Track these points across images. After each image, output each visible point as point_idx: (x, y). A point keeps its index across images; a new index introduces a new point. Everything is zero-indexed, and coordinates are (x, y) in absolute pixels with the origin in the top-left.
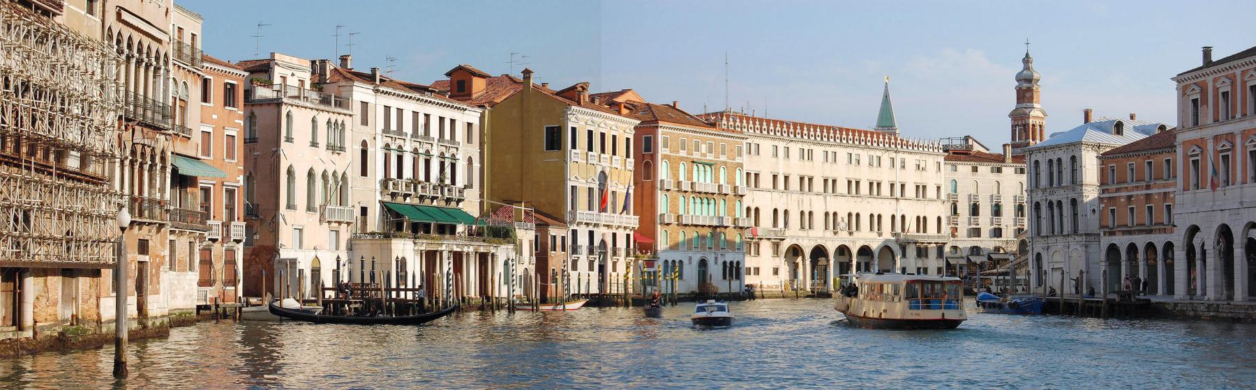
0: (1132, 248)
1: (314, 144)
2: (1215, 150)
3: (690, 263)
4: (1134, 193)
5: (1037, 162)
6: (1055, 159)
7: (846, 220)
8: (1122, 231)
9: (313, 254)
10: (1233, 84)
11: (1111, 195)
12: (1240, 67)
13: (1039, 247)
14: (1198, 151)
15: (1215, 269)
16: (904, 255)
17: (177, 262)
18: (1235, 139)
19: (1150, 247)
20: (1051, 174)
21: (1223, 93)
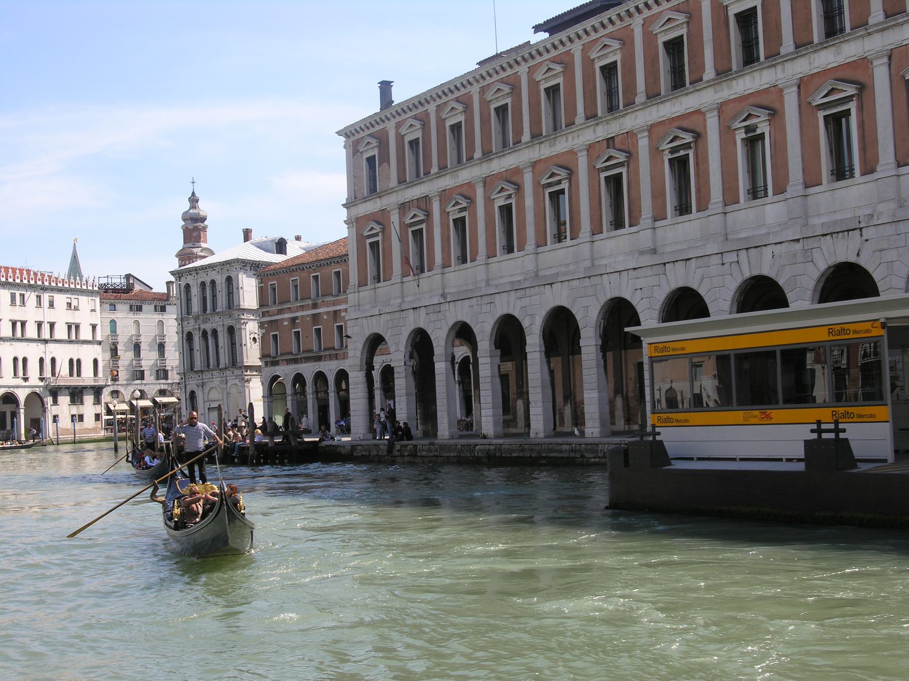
2: (402, 223)
4: (299, 314)
5: (188, 287)
8: (286, 360)
10: (425, 127)
11: (273, 318)
12: (435, 101)
13: (192, 385)
14: (378, 229)
15: (407, 394)
16: (55, 402)
17: (290, 420)
18: (431, 205)
19: (320, 377)
20: (204, 299)
21: (411, 143)
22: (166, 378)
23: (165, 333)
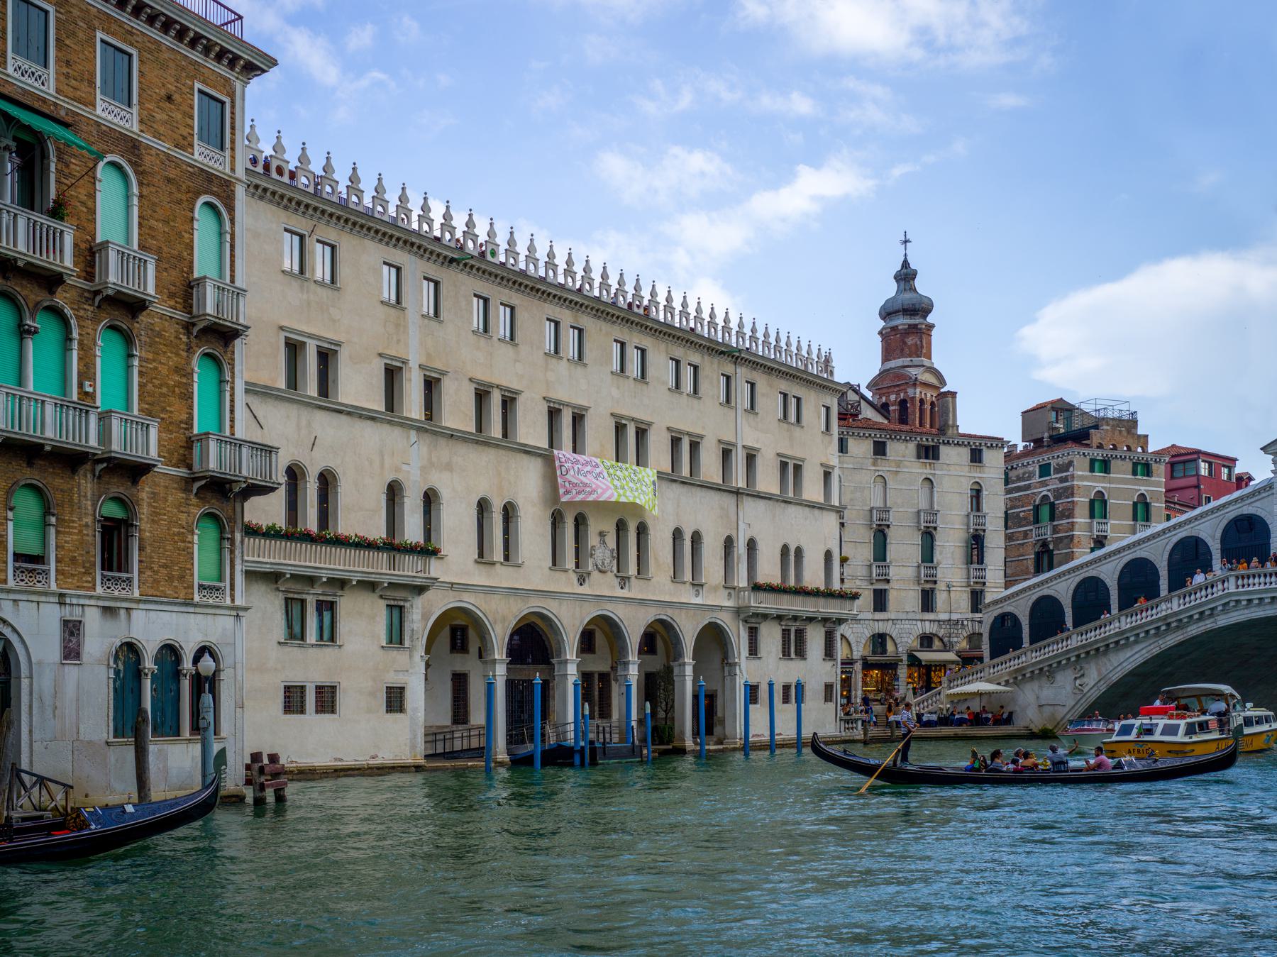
0: (270, 558)
16: (754, 651)
23: (936, 507)
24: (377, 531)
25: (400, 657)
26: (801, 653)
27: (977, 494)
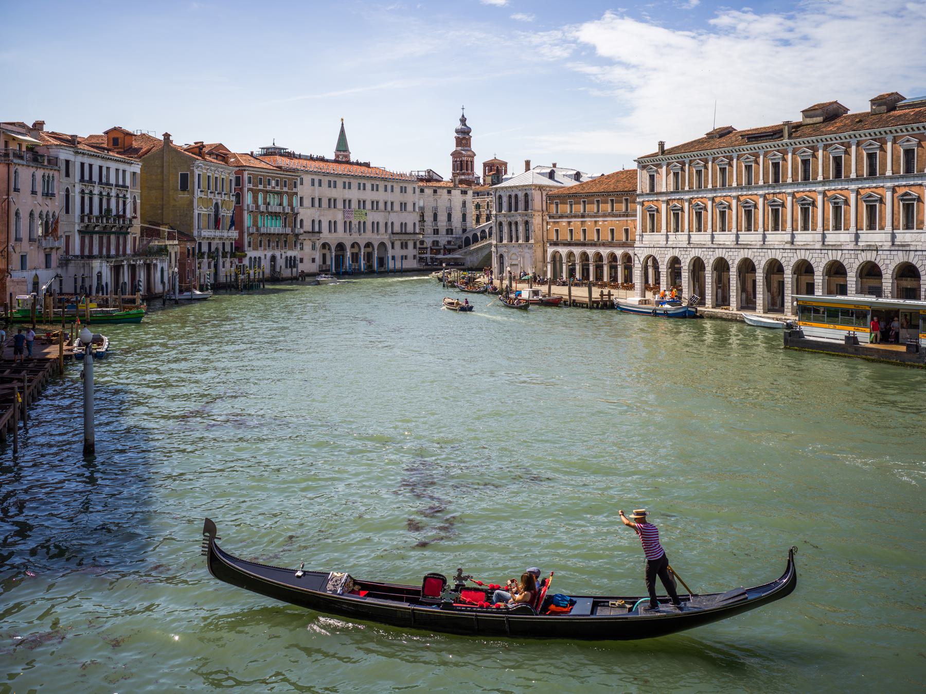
1: (34, 192)
3: (265, 258)
6: (513, 194)
7: (357, 226)
9: (34, 272)
16: (393, 248)
22: (452, 234)
24: (310, 230)
25: (314, 252)
26: (406, 248)
27: (464, 203)
